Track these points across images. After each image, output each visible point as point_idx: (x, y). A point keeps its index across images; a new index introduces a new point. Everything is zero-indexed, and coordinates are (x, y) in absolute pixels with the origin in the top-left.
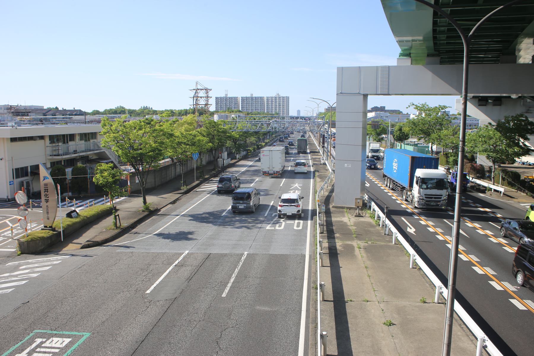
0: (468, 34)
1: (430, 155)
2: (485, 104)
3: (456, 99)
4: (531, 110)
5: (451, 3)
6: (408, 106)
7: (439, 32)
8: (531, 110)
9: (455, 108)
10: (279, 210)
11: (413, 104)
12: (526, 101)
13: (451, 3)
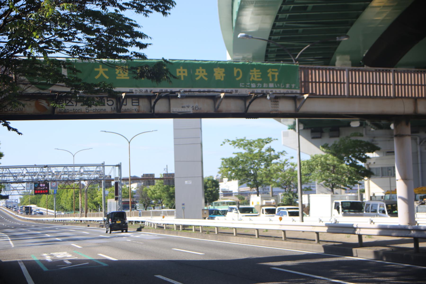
0: (297, 53)
1: (279, 202)
2: (320, 136)
3: (283, 132)
4: (376, 141)
5: (290, 10)
6: (222, 143)
7: (271, 51)
8: (376, 141)
9: (282, 144)
10: (79, 211)
11: (229, 141)
12: (370, 130)
13: (290, 10)
